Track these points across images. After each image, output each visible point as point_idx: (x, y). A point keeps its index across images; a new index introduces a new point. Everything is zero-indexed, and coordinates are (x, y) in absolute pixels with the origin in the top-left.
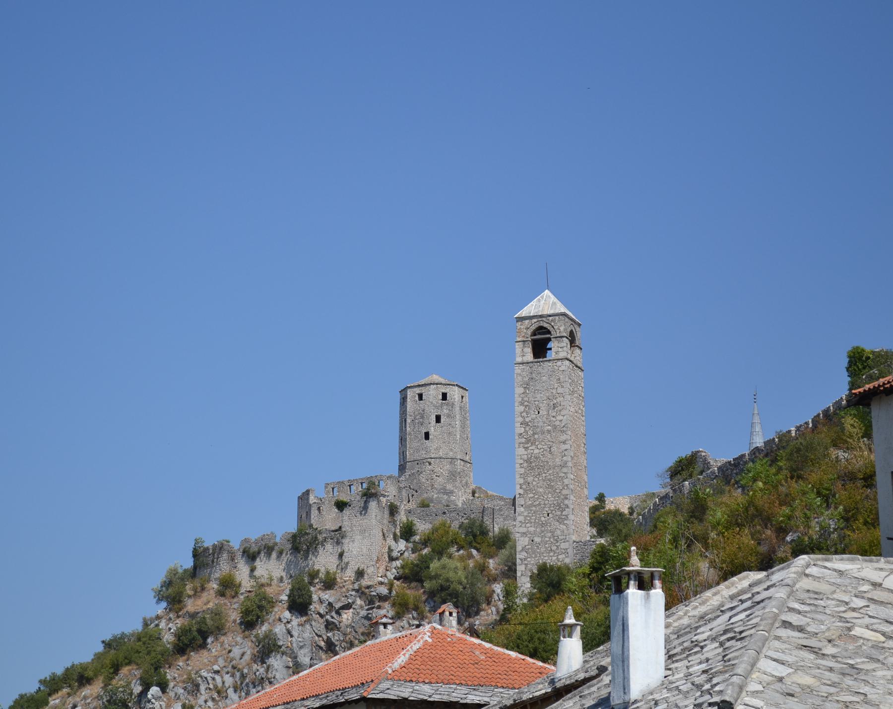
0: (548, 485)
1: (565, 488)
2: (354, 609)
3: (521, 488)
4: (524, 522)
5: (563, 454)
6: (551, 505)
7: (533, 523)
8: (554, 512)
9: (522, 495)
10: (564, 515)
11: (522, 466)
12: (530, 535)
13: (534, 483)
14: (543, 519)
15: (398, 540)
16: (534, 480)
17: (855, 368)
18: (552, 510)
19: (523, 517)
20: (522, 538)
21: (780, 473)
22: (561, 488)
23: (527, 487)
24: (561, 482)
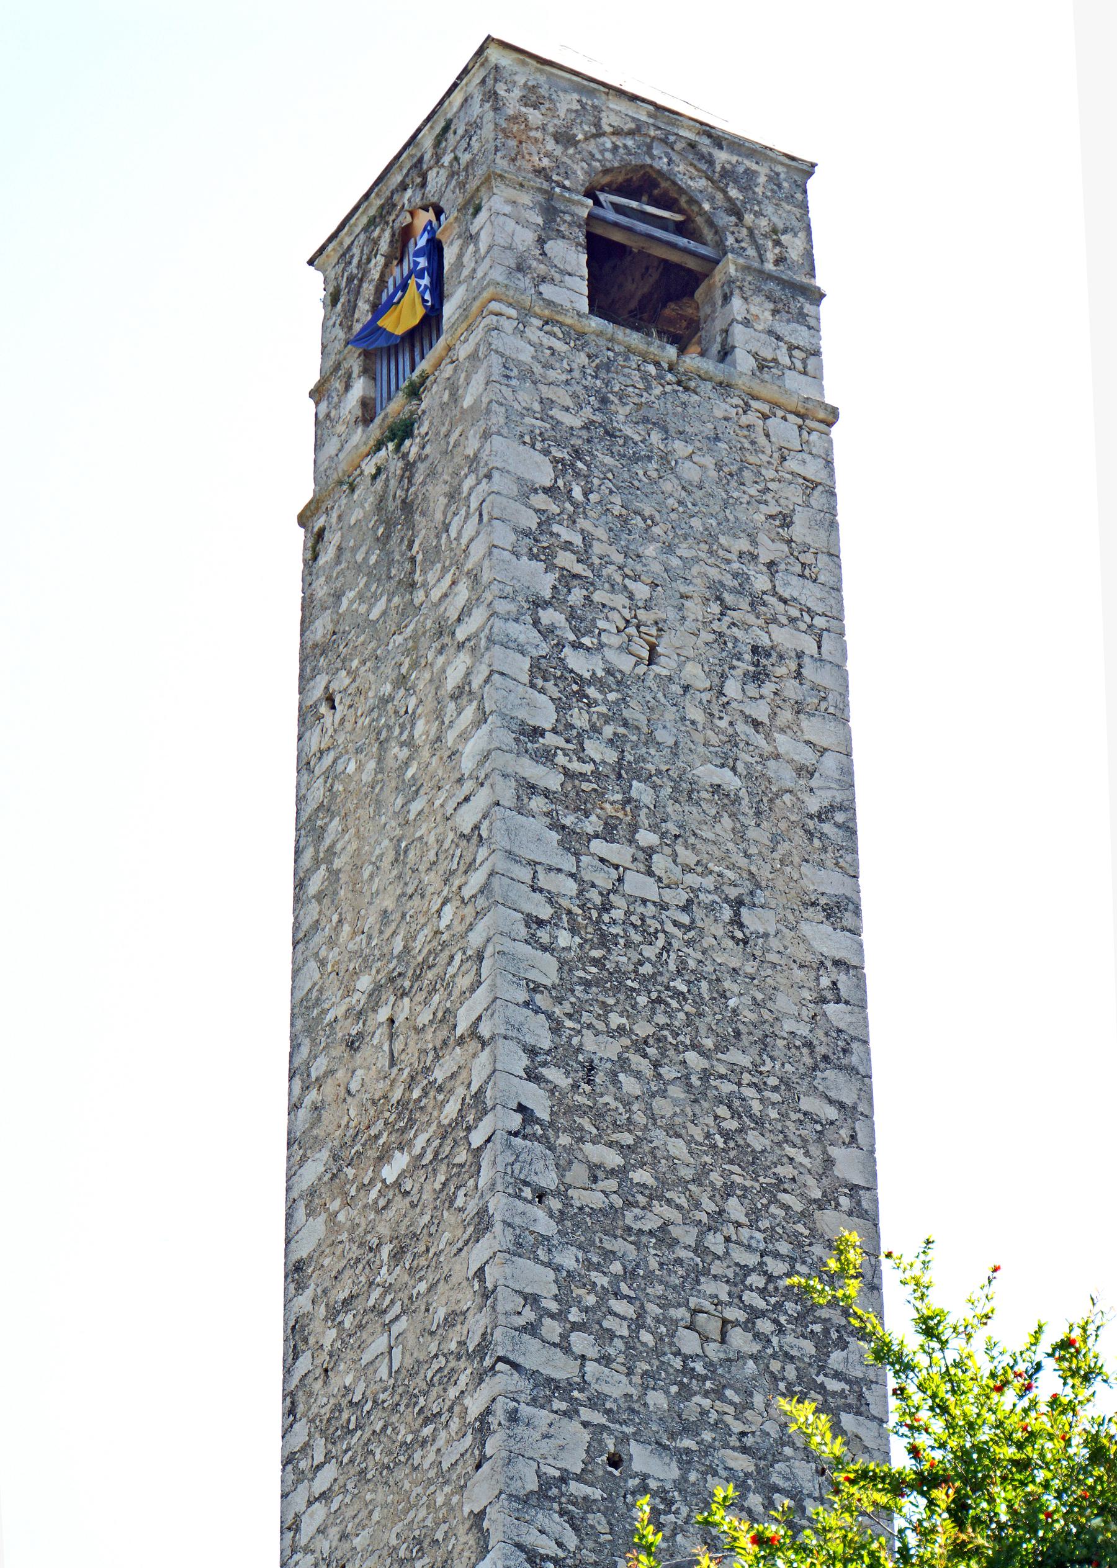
0: (726, 1135)
1: (845, 1202)
2: (380, 1024)
3: (532, 1076)
4: (553, 1306)
5: (825, 982)
6: (746, 1271)
7: (618, 1343)
8: (765, 1326)
9: (538, 1121)
10: (837, 1375)
11: (544, 936)
12: (598, 1418)
13: (629, 1084)
14: (689, 1342)
15: (357, 346)
16: (623, 1063)
17: (464, 1379)
18: (755, 1314)
19: (551, 1275)
20: (543, 1416)
21: (970, 1559)
22: (817, 1194)
23: (575, 1087)
24: (815, 1150)
